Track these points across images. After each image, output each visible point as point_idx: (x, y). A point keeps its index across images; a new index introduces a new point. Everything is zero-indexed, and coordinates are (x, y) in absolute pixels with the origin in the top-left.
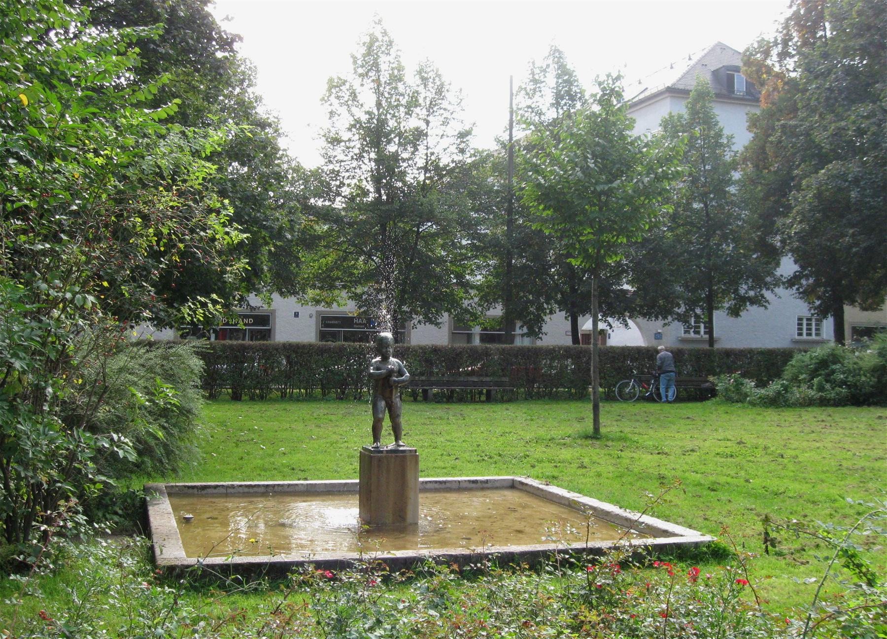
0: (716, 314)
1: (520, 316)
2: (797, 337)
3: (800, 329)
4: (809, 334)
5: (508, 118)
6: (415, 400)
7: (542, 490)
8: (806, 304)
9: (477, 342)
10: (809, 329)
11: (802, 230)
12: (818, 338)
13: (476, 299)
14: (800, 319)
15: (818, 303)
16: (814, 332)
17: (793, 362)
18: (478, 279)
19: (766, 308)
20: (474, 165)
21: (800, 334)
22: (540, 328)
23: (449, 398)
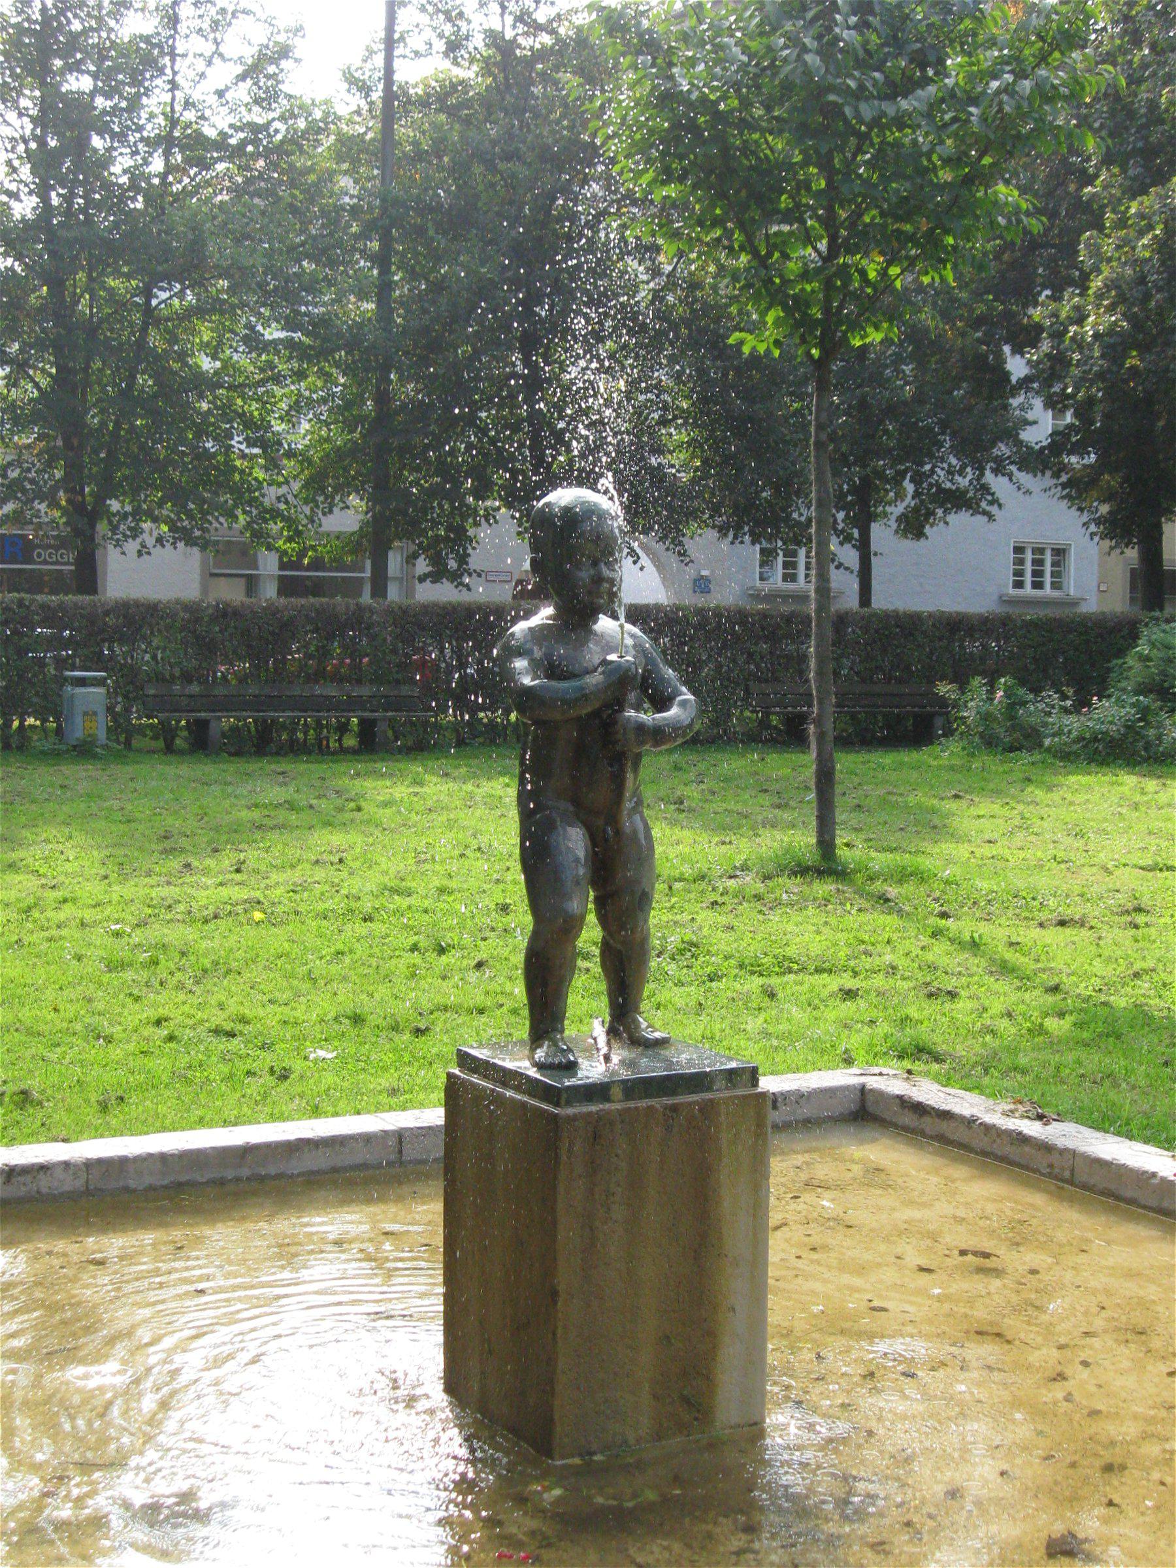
0: (876, 529)
1: (412, 529)
2: (1012, 592)
3: (1019, 573)
4: (1037, 585)
5: (382, 23)
6: (169, 749)
7: (1022, 1139)
8: (1074, 512)
9: (270, 591)
10: (1037, 574)
11: (1111, 331)
12: (1056, 594)
13: (296, 486)
14: (1019, 550)
15: (1104, 509)
16: (1048, 579)
17: (1143, 648)
18: (302, 434)
19: (990, 517)
20: (294, 142)
21: (1019, 585)
22: (463, 559)
23: (263, 743)
